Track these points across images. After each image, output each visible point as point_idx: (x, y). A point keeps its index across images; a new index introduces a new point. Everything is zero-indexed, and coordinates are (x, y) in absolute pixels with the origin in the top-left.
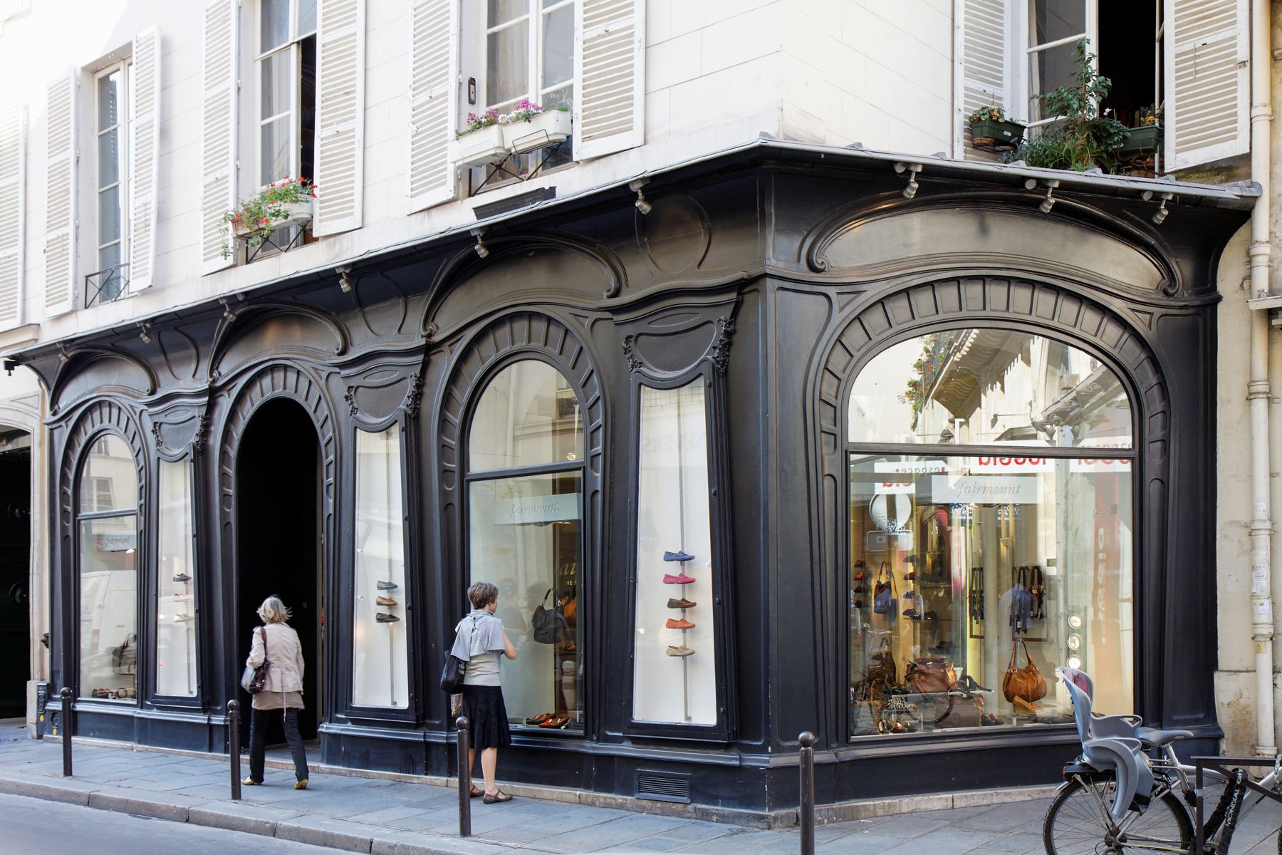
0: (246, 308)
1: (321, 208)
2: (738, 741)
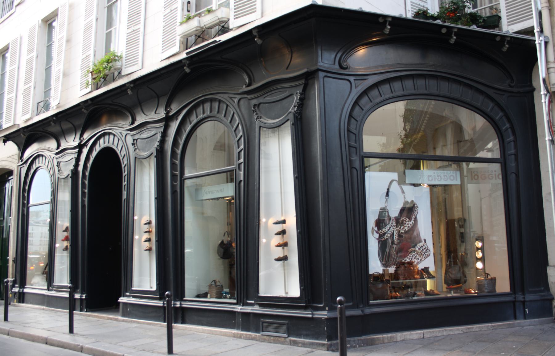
0: (93, 108)
2: (311, 304)
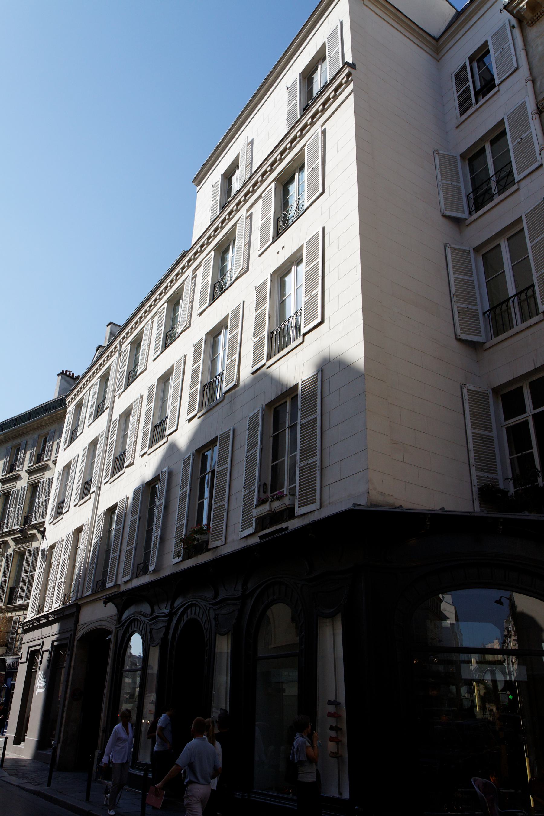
1: (212, 537)
